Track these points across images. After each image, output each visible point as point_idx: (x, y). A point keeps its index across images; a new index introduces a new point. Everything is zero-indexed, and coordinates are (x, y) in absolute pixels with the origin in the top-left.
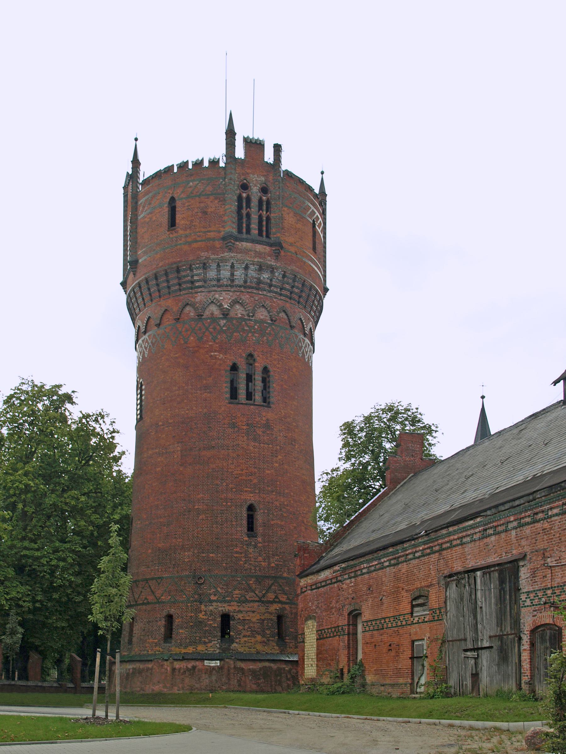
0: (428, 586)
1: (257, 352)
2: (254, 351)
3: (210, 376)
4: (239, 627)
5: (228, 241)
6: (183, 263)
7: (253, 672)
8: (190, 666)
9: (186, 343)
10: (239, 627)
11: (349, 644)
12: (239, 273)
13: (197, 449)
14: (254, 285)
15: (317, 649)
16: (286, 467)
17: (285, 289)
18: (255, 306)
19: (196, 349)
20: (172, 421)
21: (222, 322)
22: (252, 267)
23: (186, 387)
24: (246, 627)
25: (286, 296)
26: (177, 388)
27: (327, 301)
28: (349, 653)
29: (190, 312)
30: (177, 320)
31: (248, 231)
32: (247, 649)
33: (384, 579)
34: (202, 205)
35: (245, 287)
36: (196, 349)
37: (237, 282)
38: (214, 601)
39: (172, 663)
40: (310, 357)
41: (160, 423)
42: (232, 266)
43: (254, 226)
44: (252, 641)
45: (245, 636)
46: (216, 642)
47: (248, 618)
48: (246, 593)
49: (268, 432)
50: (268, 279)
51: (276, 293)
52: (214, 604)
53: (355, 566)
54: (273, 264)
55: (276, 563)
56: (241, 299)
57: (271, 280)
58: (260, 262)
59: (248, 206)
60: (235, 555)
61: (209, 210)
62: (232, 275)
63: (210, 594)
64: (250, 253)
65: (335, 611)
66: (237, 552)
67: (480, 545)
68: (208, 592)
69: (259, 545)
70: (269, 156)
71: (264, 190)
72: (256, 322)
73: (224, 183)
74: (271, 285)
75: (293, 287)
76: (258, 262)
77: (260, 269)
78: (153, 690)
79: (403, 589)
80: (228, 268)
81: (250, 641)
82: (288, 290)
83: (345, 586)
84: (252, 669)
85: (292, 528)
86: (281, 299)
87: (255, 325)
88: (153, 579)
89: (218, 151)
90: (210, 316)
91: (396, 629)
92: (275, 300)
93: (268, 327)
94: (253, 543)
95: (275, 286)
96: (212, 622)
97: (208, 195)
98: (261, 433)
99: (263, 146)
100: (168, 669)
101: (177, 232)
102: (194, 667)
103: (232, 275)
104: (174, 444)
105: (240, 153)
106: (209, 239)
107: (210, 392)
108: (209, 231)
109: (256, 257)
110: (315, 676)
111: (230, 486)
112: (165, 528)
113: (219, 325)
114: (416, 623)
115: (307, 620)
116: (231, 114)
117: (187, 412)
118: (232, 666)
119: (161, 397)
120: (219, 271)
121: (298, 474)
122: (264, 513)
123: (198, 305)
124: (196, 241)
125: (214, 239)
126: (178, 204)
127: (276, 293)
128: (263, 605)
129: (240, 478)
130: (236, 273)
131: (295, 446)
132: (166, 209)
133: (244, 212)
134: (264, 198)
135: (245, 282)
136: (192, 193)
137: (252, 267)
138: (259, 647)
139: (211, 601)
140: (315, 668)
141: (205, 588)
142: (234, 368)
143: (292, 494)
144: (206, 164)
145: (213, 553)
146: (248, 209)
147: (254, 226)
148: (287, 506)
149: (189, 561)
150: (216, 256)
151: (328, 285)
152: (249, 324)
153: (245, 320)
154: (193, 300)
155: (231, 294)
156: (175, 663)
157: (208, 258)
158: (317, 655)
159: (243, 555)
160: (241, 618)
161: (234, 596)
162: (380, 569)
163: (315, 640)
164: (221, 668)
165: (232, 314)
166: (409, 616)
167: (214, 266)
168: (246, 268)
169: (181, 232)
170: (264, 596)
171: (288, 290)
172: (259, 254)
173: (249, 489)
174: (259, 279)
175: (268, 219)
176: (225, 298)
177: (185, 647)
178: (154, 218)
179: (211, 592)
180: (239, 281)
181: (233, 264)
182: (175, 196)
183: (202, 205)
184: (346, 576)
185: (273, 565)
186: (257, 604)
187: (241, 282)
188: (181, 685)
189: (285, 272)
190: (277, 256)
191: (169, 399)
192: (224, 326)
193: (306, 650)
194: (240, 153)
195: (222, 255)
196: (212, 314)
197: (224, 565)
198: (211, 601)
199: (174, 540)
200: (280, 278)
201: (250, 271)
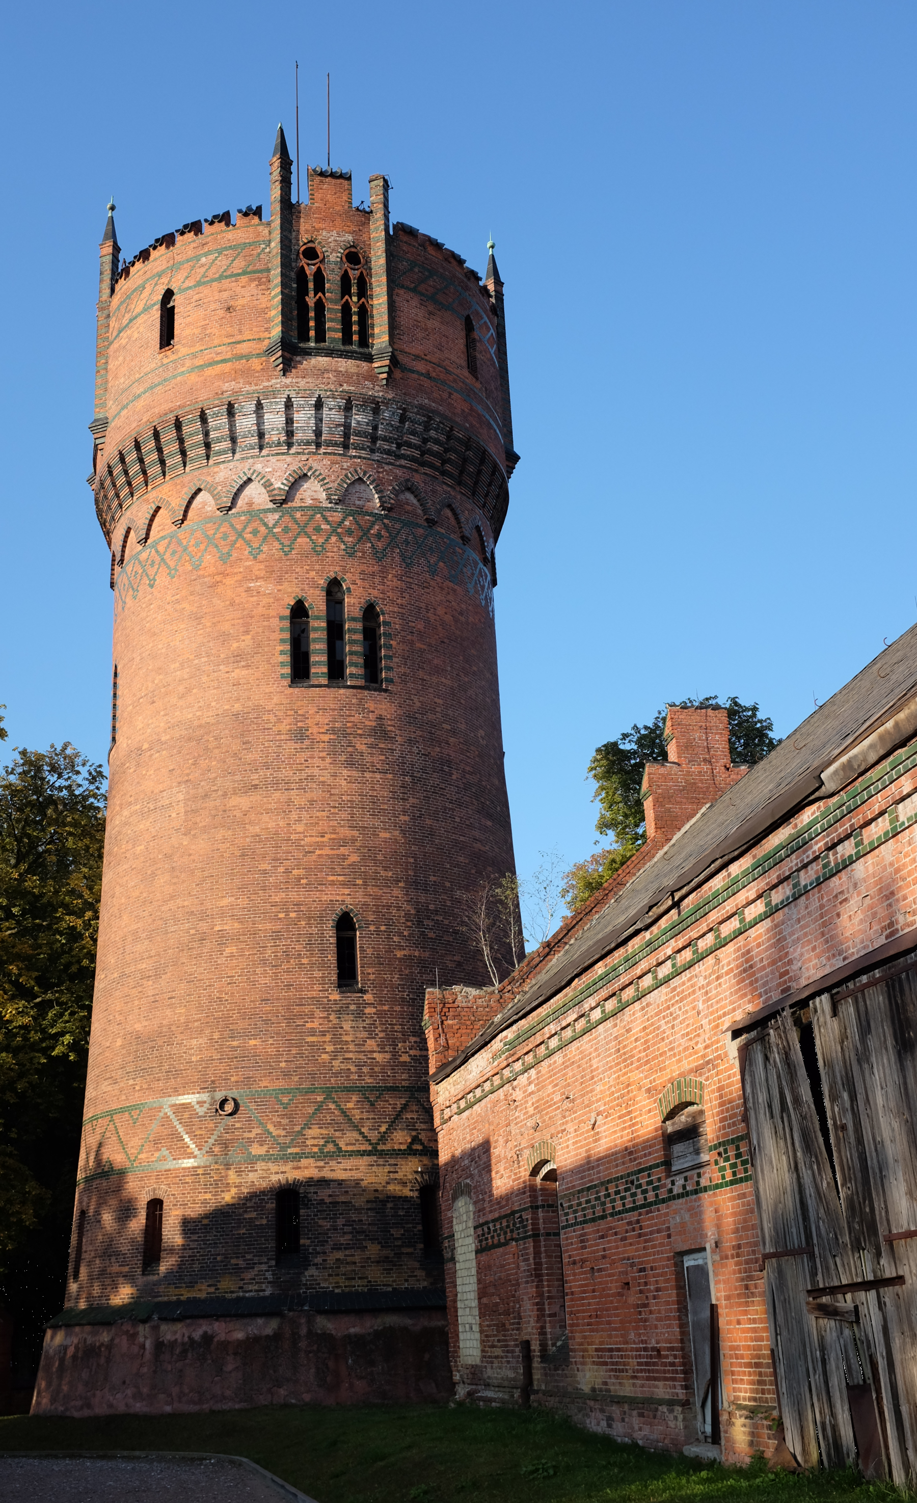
0: (697, 1070)
1: (349, 575)
4: (321, 1222)
6: (187, 409)
7: (358, 1342)
8: (197, 1335)
10: (321, 1222)
11: (538, 1264)
13: (220, 793)
15: (479, 1281)
16: (428, 822)
17: (409, 445)
19: (218, 578)
20: (168, 737)
21: (272, 518)
23: (196, 662)
24: (340, 1222)
25: (413, 459)
26: (177, 665)
27: (518, 484)
28: (540, 1295)
32: (342, 1281)
33: (595, 1063)
34: (225, 295)
36: (218, 578)
38: (260, 1158)
39: (156, 1328)
40: (489, 600)
41: (146, 746)
42: (289, 405)
43: (333, 326)
44: (357, 1259)
45: (337, 1247)
46: (264, 1267)
47: (342, 1199)
48: (338, 1134)
49: (382, 746)
50: (368, 424)
51: (388, 452)
52: (260, 1165)
53: (532, 1032)
55: (412, 1052)
56: (310, 468)
60: (310, 1039)
61: (241, 302)
62: (289, 421)
63: (250, 1141)
64: (326, 375)
65: (505, 1169)
66: (312, 1032)
67: (822, 907)
68: (246, 1135)
69: (367, 1011)
73: (268, 250)
75: (425, 441)
78: (111, 1406)
79: (640, 1088)
80: (281, 407)
81: (349, 1259)
82: (417, 447)
83: (518, 1095)
84: (356, 1335)
85: (450, 965)
86: (401, 466)
88: (122, 1111)
90: (245, 508)
91: (633, 1216)
93: (373, 523)
94: (353, 1007)
95: (385, 439)
96: (254, 1215)
97: (239, 275)
98: (364, 747)
100: (148, 1344)
102: (207, 1339)
103: (289, 421)
104: (171, 788)
106: (240, 357)
107: (247, 666)
110: (478, 1362)
111: (295, 872)
112: (150, 983)
113: (265, 525)
114: (679, 1196)
115: (455, 1198)
117: (198, 714)
118: (304, 1331)
119: (147, 689)
121: (462, 838)
122: (378, 932)
123: (220, 488)
125: (248, 357)
126: (177, 301)
127: (388, 452)
128: (381, 1161)
129: (318, 852)
130: (296, 416)
131: (451, 774)
132: (156, 314)
133: (311, 300)
135: (318, 433)
136: (204, 276)
137: (331, 403)
138: (376, 1274)
139: (253, 1160)
140: (478, 1336)
141: (238, 1125)
142: (299, 611)
143: (448, 884)
145: (255, 1036)
146: (320, 294)
147: (333, 326)
148: (436, 912)
149: (202, 1060)
150: (254, 388)
151: (517, 449)
152: (330, 519)
154: (209, 479)
156: (164, 1327)
158: (479, 1299)
159: (328, 1038)
160: (328, 1200)
161: (309, 1142)
162: (585, 1032)
163: (473, 1255)
164: (277, 1337)
166: (659, 1173)
168: (319, 405)
170: (383, 1138)
171: (417, 447)
173: (341, 878)
177: (191, 1285)
178: (136, 335)
179: (252, 1135)
181: (289, 399)
182: (174, 287)
183: (225, 295)
184: (518, 1066)
185: (405, 1058)
186: (366, 1160)
188: (175, 1391)
189: (404, 410)
191: (163, 690)
192: (274, 526)
193: (459, 1281)
195: (266, 384)
197: (283, 1065)
198: (253, 1160)
199: (168, 1012)
200: (395, 422)
201: (325, 411)
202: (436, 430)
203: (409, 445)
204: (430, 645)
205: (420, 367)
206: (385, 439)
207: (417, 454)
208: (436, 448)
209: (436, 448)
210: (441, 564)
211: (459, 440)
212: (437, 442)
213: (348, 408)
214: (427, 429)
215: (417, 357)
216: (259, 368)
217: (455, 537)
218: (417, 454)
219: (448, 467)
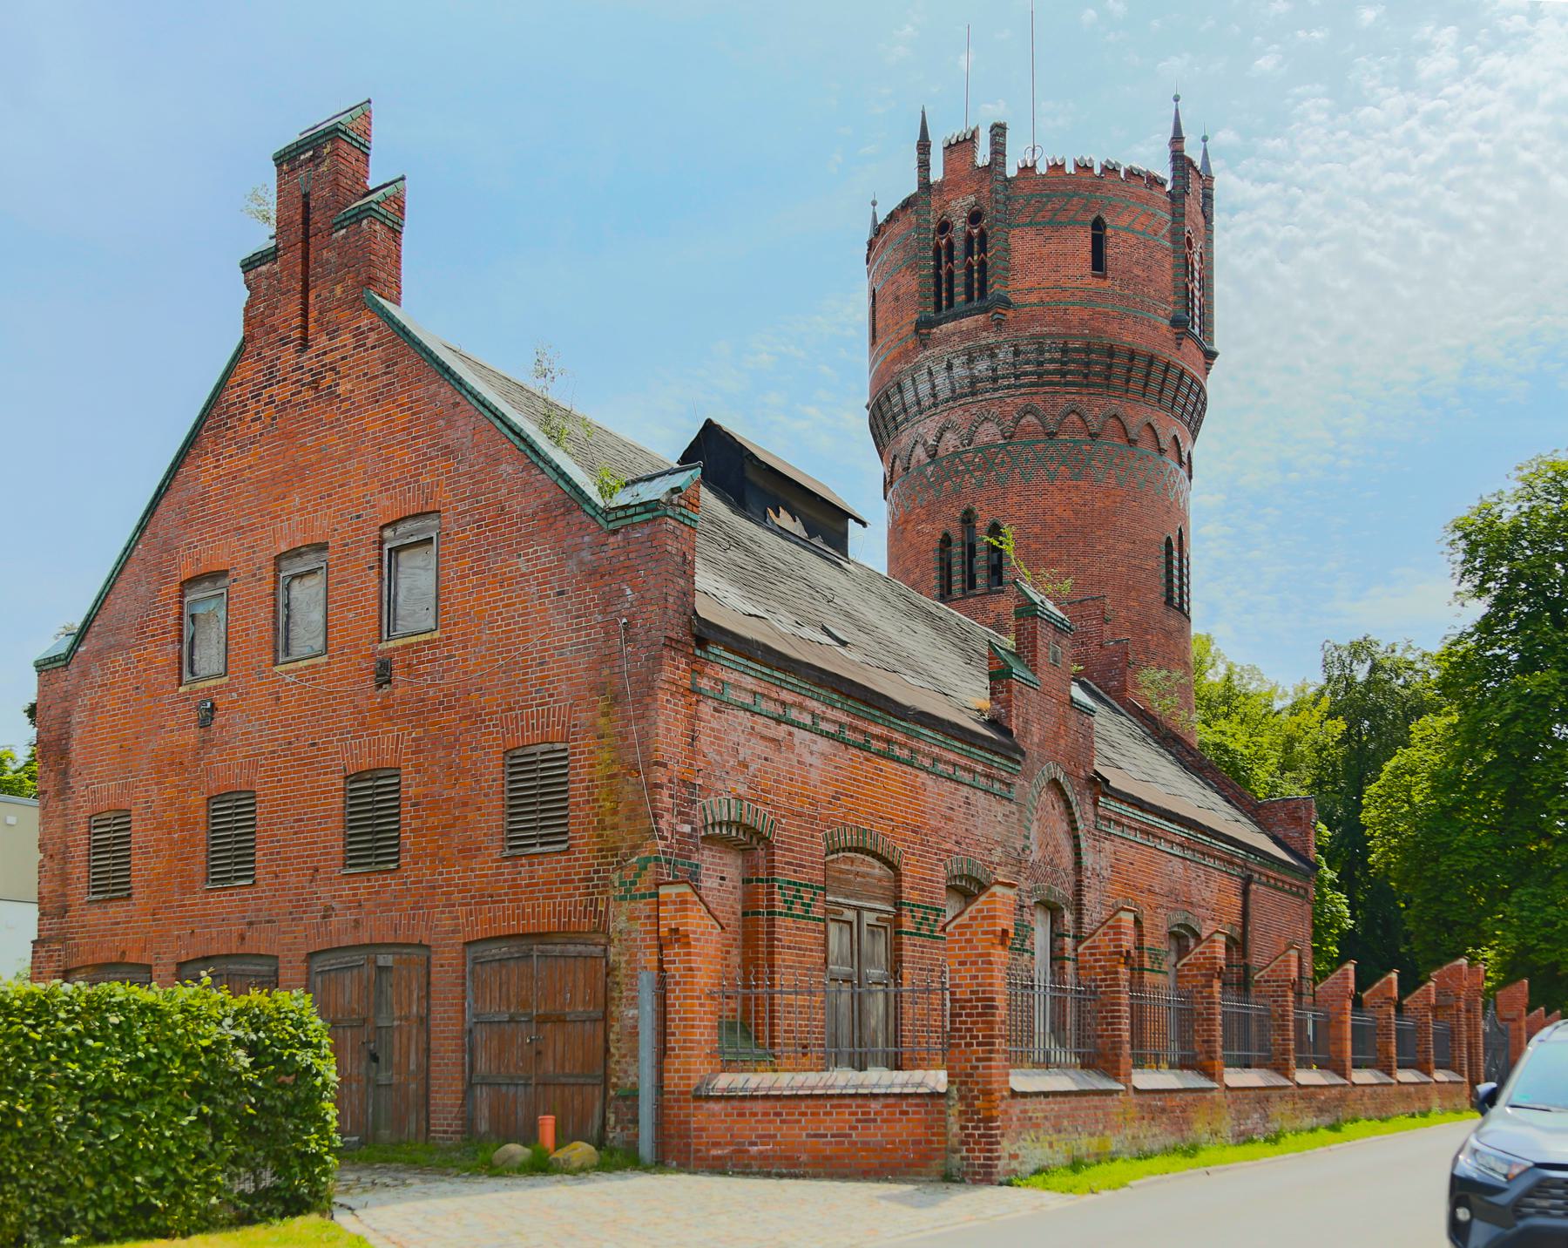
12: (941, 380)
14: (967, 390)
17: (1026, 374)
22: (956, 362)
31: (951, 304)
37: (941, 396)
42: (930, 373)
51: (1008, 387)
57: (994, 370)
59: (950, 258)
62: (934, 387)
70: (983, 156)
71: (975, 217)
72: (977, 450)
74: (995, 380)
75: (1040, 364)
80: (926, 377)
103: (934, 387)
105: (936, 175)
127: (1008, 387)
135: (953, 391)
142: (946, 541)
144: (1070, 169)
168: (950, 367)
172: (967, 335)
175: (983, 264)
194: (936, 175)
201: (955, 370)
203: (1026, 374)
204: (1045, 543)
205: (1033, 298)
207: (1034, 378)
208: (1051, 367)
209: (1051, 367)
211: (1076, 350)
212: (1052, 361)
213: (971, 360)
214: (1041, 352)
215: (1030, 290)
217: (1084, 437)
218: (1034, 378)
219: (1069, 378)
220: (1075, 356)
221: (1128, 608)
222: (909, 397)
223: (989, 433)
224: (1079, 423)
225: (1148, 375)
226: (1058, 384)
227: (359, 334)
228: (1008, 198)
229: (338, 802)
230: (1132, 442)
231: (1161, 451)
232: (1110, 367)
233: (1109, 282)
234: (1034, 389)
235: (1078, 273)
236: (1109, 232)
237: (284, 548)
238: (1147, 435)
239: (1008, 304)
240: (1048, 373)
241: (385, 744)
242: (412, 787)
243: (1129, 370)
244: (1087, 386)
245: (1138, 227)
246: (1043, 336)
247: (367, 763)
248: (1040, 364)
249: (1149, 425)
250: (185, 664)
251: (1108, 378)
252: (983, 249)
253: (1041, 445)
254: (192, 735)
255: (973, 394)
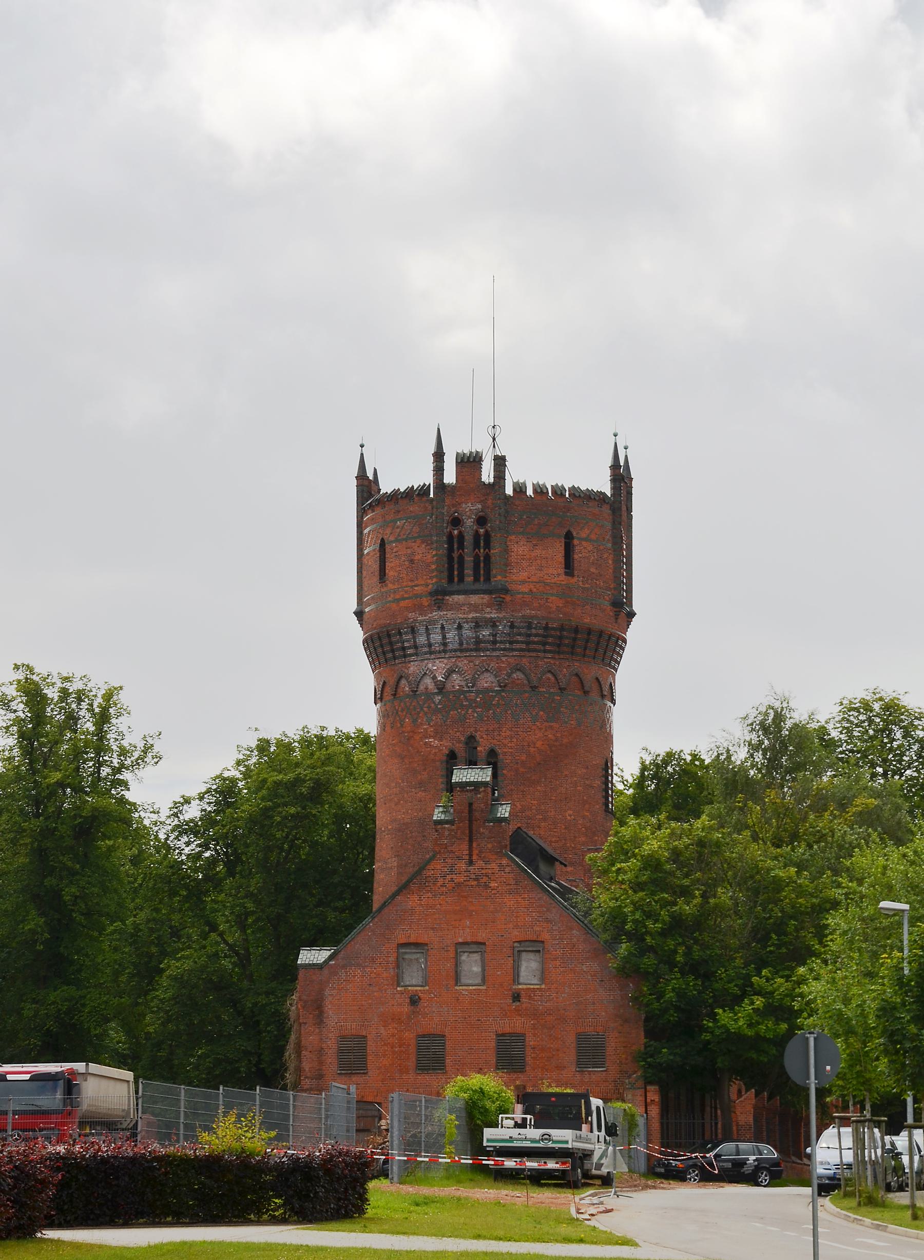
2: (476, 731)
3: (425, 770)
5: (439, 597)
9: (402, 725)
12: (451, 635)
14: (472, 646)
17: (518, 642)
18: (476, 673)
21: (438, 698)
22: (466, 626)
29: (405, 686)
30: (395, 695)
31: (461, 579)
34: (409, 551)
35: (461, 651)
37: (450, 646)
42: (443, 628)
51: (504, 649)
54: (493, 616)
58: (476, 618)
61: (416, 558)
62: (444, 637)
70: (487, 474)
71: (481, 521)
72: (478, 692)
74: (495, 642)
76: (473, 618)
77: (478, 625)
80: (438, 630)
87: (477, 697)
89: (427, 478)
92: (504, 659)
95: (501, 642)
99: (481, 459)
101: (386, 586)
103: (444, 637)
105: (450, 477)
106: (416, 596)
107: (425, 791)
108: (416, 586)
109: (470, 612)
116: (439, 429)
120: (428, 635)
124: (404, 599)
127: (504, 649)
133: (455, 555)
134: (482, 531)
135: (461, 644)
147: (469, 571)
153: (464, 692)
155: (445, 661)
157: (415, 621)
165: (448, 686)
167: (422, 630)
168: (460, 627)
169: (390, 586)
172: (475, 608)
174: (477, 637)
175: (487, 558)
176: (439, 667)
180: (453, 645)
181: (442, 625)
183: (409, 551)
187: (456, 646)
190: (500, 605)
194: (450, 477)
196: (426, 688)
202: (535, 628)
203: (518, 642)
206: (501, 642)
210: (542, 713)
211: (553, 629)
212: (536, 635)
215: (523, 582)
216: (427, 604)
220: (553, 632)
221: (584, 817)
222: (422, 640)
223: (487, 681)
224: (553, 678)
225: (598, 643)
226: (539, 651)
227: (500, 865)
228: (507, 512)
229: (493, 1044)
230: (586, 693)
231: (603, 696)
232: (575, 639)
233: (575, 579)
234: (522, 654)
235: (555, 572)
236: (576, 542)
237: (460, 940)
238: (595, 687)
239: (506, 591)
240: (534, 643)
241: (517, 1024)
242: (531, 1041)
243: (587, 641)
244: (559, 653)
245: (593, 537)
246: (532, 617)
247: (508, 1030)
248: (529, 635)
249: (597, 679)
250: (398, 980)
251: (573, 647)
252: (488, 545)
253: (527, 695)
254: (406, 1008)
255: (477, 650)
